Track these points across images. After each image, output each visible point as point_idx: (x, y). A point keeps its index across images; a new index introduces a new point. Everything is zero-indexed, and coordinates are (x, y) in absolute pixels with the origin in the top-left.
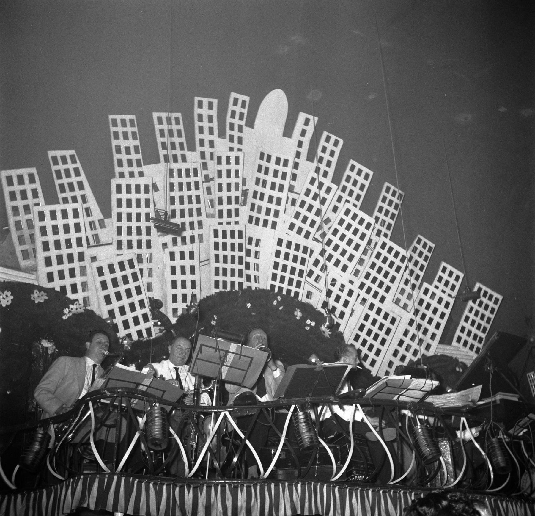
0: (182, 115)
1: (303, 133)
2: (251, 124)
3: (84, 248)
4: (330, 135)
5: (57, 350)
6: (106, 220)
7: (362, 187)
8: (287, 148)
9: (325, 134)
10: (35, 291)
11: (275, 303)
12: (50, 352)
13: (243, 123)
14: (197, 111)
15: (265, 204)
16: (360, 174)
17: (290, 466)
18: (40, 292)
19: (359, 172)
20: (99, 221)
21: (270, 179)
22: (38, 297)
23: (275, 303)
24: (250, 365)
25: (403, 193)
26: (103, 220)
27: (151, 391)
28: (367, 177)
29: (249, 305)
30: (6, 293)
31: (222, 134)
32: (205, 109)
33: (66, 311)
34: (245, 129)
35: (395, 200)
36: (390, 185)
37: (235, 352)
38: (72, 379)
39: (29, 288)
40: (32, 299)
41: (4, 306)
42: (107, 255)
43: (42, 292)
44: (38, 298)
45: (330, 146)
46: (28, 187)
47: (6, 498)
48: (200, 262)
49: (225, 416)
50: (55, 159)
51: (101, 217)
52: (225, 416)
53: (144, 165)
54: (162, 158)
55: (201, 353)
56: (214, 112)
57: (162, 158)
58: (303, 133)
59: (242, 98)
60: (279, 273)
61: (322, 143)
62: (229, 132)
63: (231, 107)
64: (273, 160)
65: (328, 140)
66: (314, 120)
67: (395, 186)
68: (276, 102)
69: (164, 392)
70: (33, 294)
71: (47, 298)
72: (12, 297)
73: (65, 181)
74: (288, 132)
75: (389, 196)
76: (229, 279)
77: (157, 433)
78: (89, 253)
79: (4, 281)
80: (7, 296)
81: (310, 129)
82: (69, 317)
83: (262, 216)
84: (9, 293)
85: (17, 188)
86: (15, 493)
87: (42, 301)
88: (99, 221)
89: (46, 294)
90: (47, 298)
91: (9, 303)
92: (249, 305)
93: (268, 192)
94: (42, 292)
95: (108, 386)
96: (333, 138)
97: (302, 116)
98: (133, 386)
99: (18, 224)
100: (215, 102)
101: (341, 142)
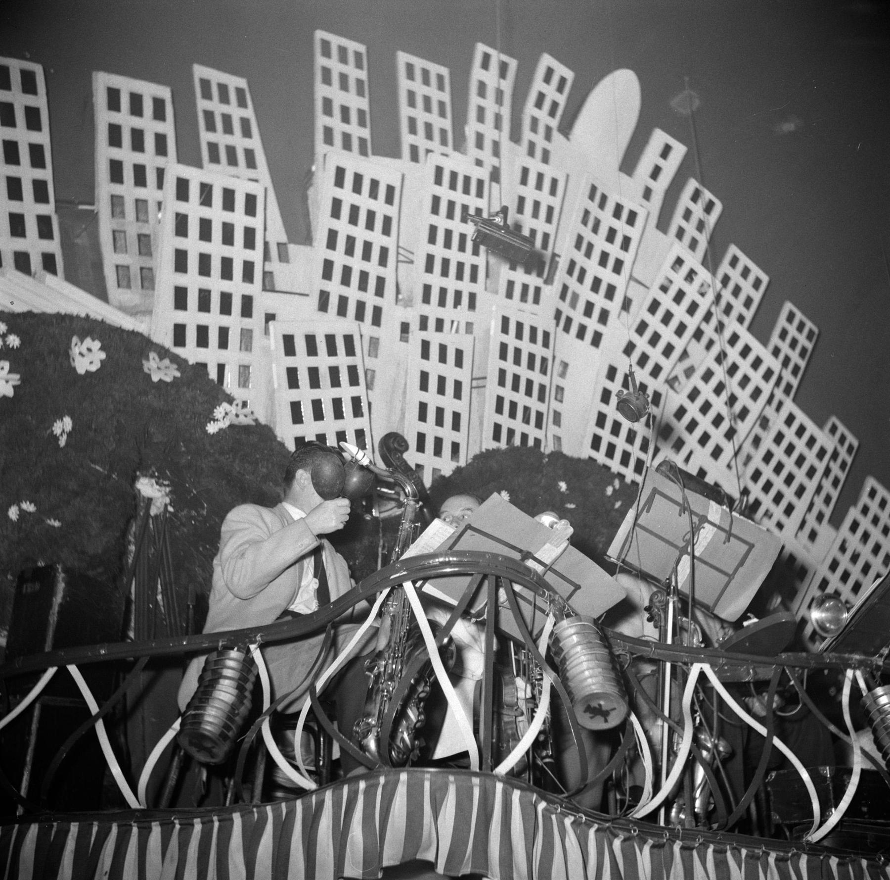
0: (451, 74)
1: (656, 173)
2: (566, 128)
3: (254, 289)
4: (701, 188)
5: (171, 509)
6: (292, 248)
7: (748, 303)
8: (627, 191)
9: (692, 184)
10: (152, 355)
11: (609, 491)
12: (153, 511)
13: (554, 123)
14: (477, 73)
15: (585, 292)
16: (747, 276)
17: (865, 813)
18: (161, 359)
19: (746, 273)
20: (279, 244)
21: (600, 243)
22: (159, 368)
23: (609, 491)
24: (741, 563)
25: (816, 330)
26: (285, 244)
27: (550, 578)
28: (757, 284)
29: (563, 486)
30: (88, 342)
31: (516, 137)
32: (490, 73)
33: (219, 412)
34: (556, 135)
35: (802, 340)
36: (795, 310)
37: (717, 522)
38: (267, 557)
39: (140, 345)
40: (146, 370)
41: (81, 370)
42: (300, 317)
43: (167, 362)
44: (159, 371)
45: (698, 210)
46: (149, 125)
47: (115, 829)
48: (472, 379)
49: (702, 676)
50: (206, 84)
51: (284, 238)
52: (702, 676)
53: (374, 154)
54: (406, 151)
55: (648, 511)
56: (507, 86)
57: (406, 151)
58: (656, 173)
59: (562, 70)
60: (606, 435)
61: (685, 200)
62: (527, 135)
63: (538, 85)
64: (610, 206)
65: (695, 197)
66: (679, 150)
67: (804, 312)
68: (618, 95)
69: (577, 587)
70: (148, 359)
71: (178, 374)
72: (103, 356)
73: (221, 139)
74: (628, 164)
75: (792, 331)
76: (518, 426)
77: (590, 681)
78: (263, 302)
79: (87, 316)
80: (89, 350)
81: (670, 167)
82: (221, 430)
83: (578, 317)
84: (97, 345)
85: (125, 119)
86: (144, 818)
87: (168, 379)
88: (279, 244)
89: (175, 366)
90: (178, 374)
91: (94, 368)
92: (563, 486)
93: (593, 268)
94: (167, 362)
95: (457, 548)
96: (707, 195)
97: (659, 138)
98: (517, 556)
99: (117, 202)
100: (513, 64)
101: (718, 208)
